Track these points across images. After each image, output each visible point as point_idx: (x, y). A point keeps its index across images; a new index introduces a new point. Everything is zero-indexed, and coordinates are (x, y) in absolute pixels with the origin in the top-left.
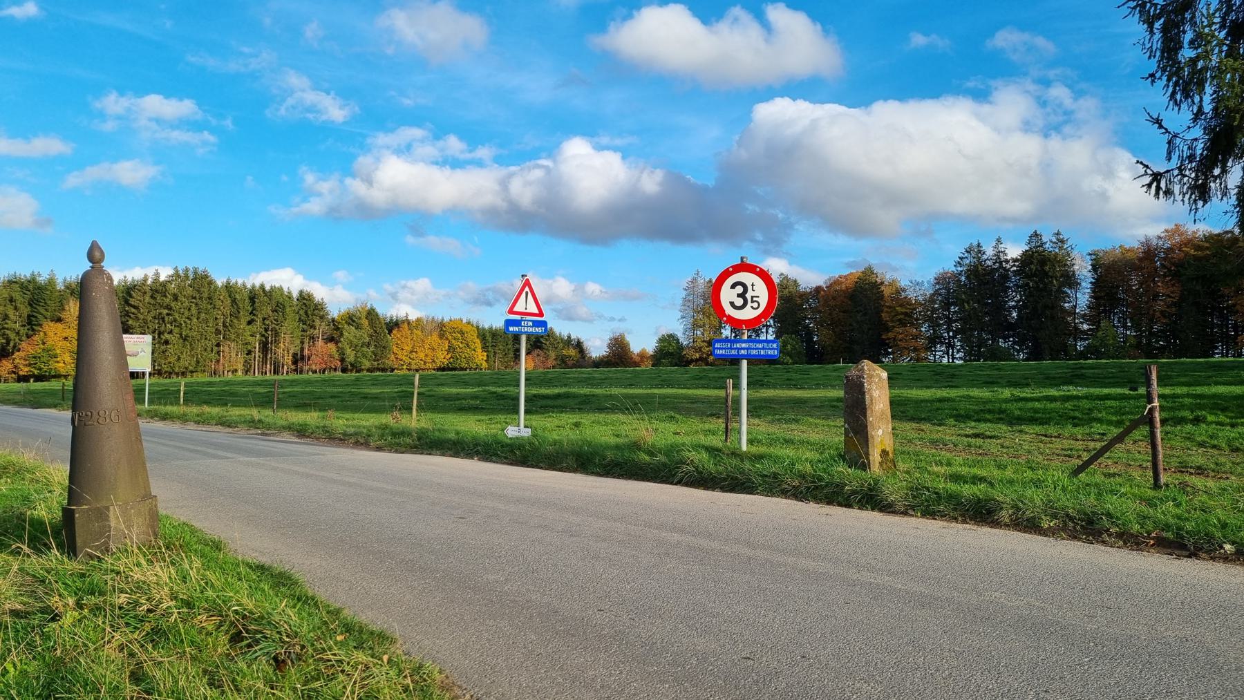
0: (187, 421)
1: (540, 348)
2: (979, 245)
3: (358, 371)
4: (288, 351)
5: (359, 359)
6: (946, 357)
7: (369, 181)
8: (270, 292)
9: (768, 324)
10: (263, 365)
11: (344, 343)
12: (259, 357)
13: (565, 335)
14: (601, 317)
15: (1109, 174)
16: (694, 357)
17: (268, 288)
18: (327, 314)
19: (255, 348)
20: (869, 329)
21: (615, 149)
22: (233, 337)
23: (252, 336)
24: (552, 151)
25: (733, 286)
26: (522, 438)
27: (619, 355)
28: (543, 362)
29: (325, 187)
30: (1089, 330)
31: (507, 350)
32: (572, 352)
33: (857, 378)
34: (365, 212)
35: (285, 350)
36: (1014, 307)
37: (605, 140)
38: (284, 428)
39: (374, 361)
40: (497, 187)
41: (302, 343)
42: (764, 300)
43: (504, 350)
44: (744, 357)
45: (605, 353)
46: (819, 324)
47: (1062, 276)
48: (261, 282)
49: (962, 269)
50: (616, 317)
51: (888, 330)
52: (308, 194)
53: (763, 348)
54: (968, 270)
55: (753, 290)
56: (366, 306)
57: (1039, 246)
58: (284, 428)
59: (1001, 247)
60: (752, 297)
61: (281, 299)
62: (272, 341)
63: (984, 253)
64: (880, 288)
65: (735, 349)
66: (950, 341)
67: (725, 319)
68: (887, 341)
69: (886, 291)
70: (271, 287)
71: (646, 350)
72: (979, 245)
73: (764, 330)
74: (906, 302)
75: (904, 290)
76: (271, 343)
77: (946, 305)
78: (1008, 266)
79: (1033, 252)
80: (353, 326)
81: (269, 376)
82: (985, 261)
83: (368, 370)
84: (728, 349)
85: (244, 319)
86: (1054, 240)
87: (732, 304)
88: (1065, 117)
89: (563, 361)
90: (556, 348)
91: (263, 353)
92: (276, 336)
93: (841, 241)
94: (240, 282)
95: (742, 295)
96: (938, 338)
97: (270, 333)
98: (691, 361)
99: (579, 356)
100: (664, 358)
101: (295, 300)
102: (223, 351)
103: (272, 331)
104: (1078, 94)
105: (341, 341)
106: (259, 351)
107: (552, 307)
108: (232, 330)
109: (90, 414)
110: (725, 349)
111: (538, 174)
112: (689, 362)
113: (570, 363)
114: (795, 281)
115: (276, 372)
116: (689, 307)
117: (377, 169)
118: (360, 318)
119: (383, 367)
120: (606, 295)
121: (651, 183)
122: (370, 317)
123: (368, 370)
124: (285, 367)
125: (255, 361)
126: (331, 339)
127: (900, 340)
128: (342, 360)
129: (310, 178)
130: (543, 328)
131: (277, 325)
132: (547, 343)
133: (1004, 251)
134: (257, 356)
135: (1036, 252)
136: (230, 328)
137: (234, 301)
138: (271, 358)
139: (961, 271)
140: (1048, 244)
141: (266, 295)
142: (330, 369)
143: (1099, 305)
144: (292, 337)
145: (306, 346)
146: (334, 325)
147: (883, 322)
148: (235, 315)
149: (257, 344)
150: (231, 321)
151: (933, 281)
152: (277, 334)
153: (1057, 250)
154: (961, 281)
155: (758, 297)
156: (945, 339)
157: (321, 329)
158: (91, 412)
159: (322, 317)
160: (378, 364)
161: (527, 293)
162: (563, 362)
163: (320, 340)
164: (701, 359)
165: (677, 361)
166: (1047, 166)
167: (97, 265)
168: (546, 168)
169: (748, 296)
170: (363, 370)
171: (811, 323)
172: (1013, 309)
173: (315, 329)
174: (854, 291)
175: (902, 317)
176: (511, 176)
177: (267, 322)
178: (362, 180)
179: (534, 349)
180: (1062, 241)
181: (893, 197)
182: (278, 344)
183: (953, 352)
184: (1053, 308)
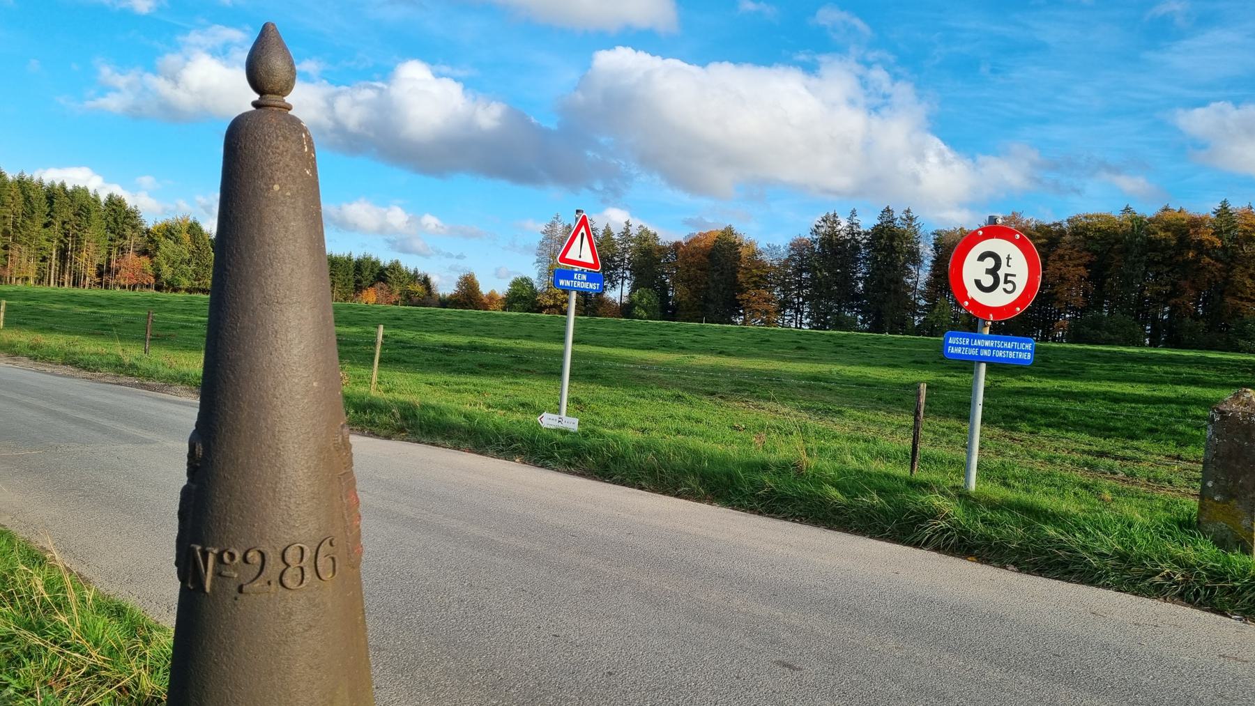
0: (17, 355)
1: (384, 281)
2: (835, 215)
3: (175, 290)
4: (91, 261)
5: (177, 277)
6: (794, 321)
7: (174, 79)
8: (72, 192)
9: (625, 275)
10: (59, 275)
11: (160, 258)
12: (56, 265)
13: (411, 269)
14: (438, 252)
15: (921, 157)
16: (548, 304)
17: (69, 187)
18: (141, 223)
19: (52, 254)
20: (724, 289)
21: (456, 80)
22: (24, 239)
23: (48, 240)
24: (386, 74)
25: (982, 257)
26: (565, 432)
27: (468, 296)
28: (386, 296)
29: (121, 81)
30: (926, 305)
31: (347, 280)
32: (418, 288)
33: (1244, 417)
34: (170, 113)
35: (88, 259)
36: (860, 279)
37: (445, 69)
38: (173, 379)
39: (195, 280)
40: (323, 104)
41: (110, 253)
42: (1021, 281)
43: (344, 280)
44: (981, 359)
45: (453, 292)
46: (675, 280)
47: (908, 252)
48: (61, 180)
49: (817, 237)
50: (454, 254)
51: (742, 291)
52: (105, 89)
53: (1013, 349)
54: (823, 239)
55: (1008, 265)
56: (188, 220)
57: (890, 222)
58: (173, 379)
59: (855, 220)
60: (1007, 275)
61: (86, 202)
62: (72, 248)
63: (839, 224)
64: (738, 249)
65: (975, 347)
66: (799, 306)
67: (967, 303)
68: (741, 302)
69: (744, 252)
70: (74, 187)
71: (495, 292)
72: (835, 215)
73: (620, 281)
74: (761, 265)
75: (760, 253)
76: (71, 251)
77: (799, 271)
78: (859, 239)
79: (883, 227)
80: (171, 239)
81: (67, 288)
82: (839, 231)
83: (188, 290)
84: (966, 346)
85: (40, 220)
86: (904, 217)
87: (978, 283)
88: (885, 101)
89: (408, 297)
90: (402, 282)
91: (60, 261)
92: (77, 244)
93: (682, 198)
94: (36, 178)
95: (993, 272)
96: (787, 302)
97: (70, 239)
98: (546, 307)
99: (425, 292)
100: (516, 302)
101: (103, 204)
102: (11, 256)
103: (72, 237)
104: (896, 78)
105: (156, 256)
106: (56, 259)
107: (386, 238)
108: (24, 233)
109: (258, 559)
110: (962, 346)
111: (367, 94)
112: (540, 310)
113: (416, 299)
114: (655, 235)
115: (76, 283)
116: (545, 251)
117: (184, 67)
118: (180, 232)
119: (205, 287)
120: (441, 230)
121: (489, 116)
122: (192, 231)
123: (188, 290)
124: (87, 278)
125: (50, 269)
126: (144, 252)
127: (753, 302)
128: (157, 277)
129: (106, 71)
130: (598, 284)
131: (79, 231)
132: (392, 276)
133: (858, 223)
134: (53, 264)
135: (887, 227)
136: (21, 230)
137: (27, 199)
138: (70, 267)
139: (817, 239)
140: (898, 220)
141: (67, 196)
142: (142, 286)
143: (937, 283)
144: (97, 246)
145: (114, 257)
146: (149, 236)
147: (739, 283)
148: (29, 215)
149: (54, 250)
150: (23, 221)
151: (788, 247)
152: (78, 241)
153: (906, 227)
154: (814, 249)
155: (1014, 275)
156: (794, 304)
157: (133, 239)
158: (263, 555)
159: (134, 227)
160: (200, 284)
161: (582, 235)
162: (408, 298)
163: (131, 251)
164: (555, 306)
165: (530, 306)
166: (868, 145)
167: (272, 99)
168: (381, 90)
169: (1001, 273)
170: (181, 289)
171: (667, 278)
172: (861, 280)
173: (125, 239)
174: (713, 250)
175: (757, 279)
176: (339, 93)
177: (67, 227)
178: (166, 78)
179: (377, 282)
180: (911, 219)
181: (727, 158)
182: (79, 253)
183: (801, 318)
184: (897, 283)
